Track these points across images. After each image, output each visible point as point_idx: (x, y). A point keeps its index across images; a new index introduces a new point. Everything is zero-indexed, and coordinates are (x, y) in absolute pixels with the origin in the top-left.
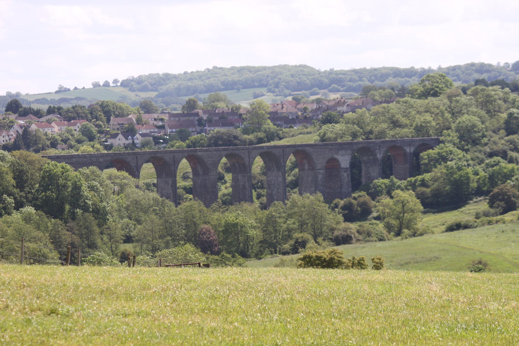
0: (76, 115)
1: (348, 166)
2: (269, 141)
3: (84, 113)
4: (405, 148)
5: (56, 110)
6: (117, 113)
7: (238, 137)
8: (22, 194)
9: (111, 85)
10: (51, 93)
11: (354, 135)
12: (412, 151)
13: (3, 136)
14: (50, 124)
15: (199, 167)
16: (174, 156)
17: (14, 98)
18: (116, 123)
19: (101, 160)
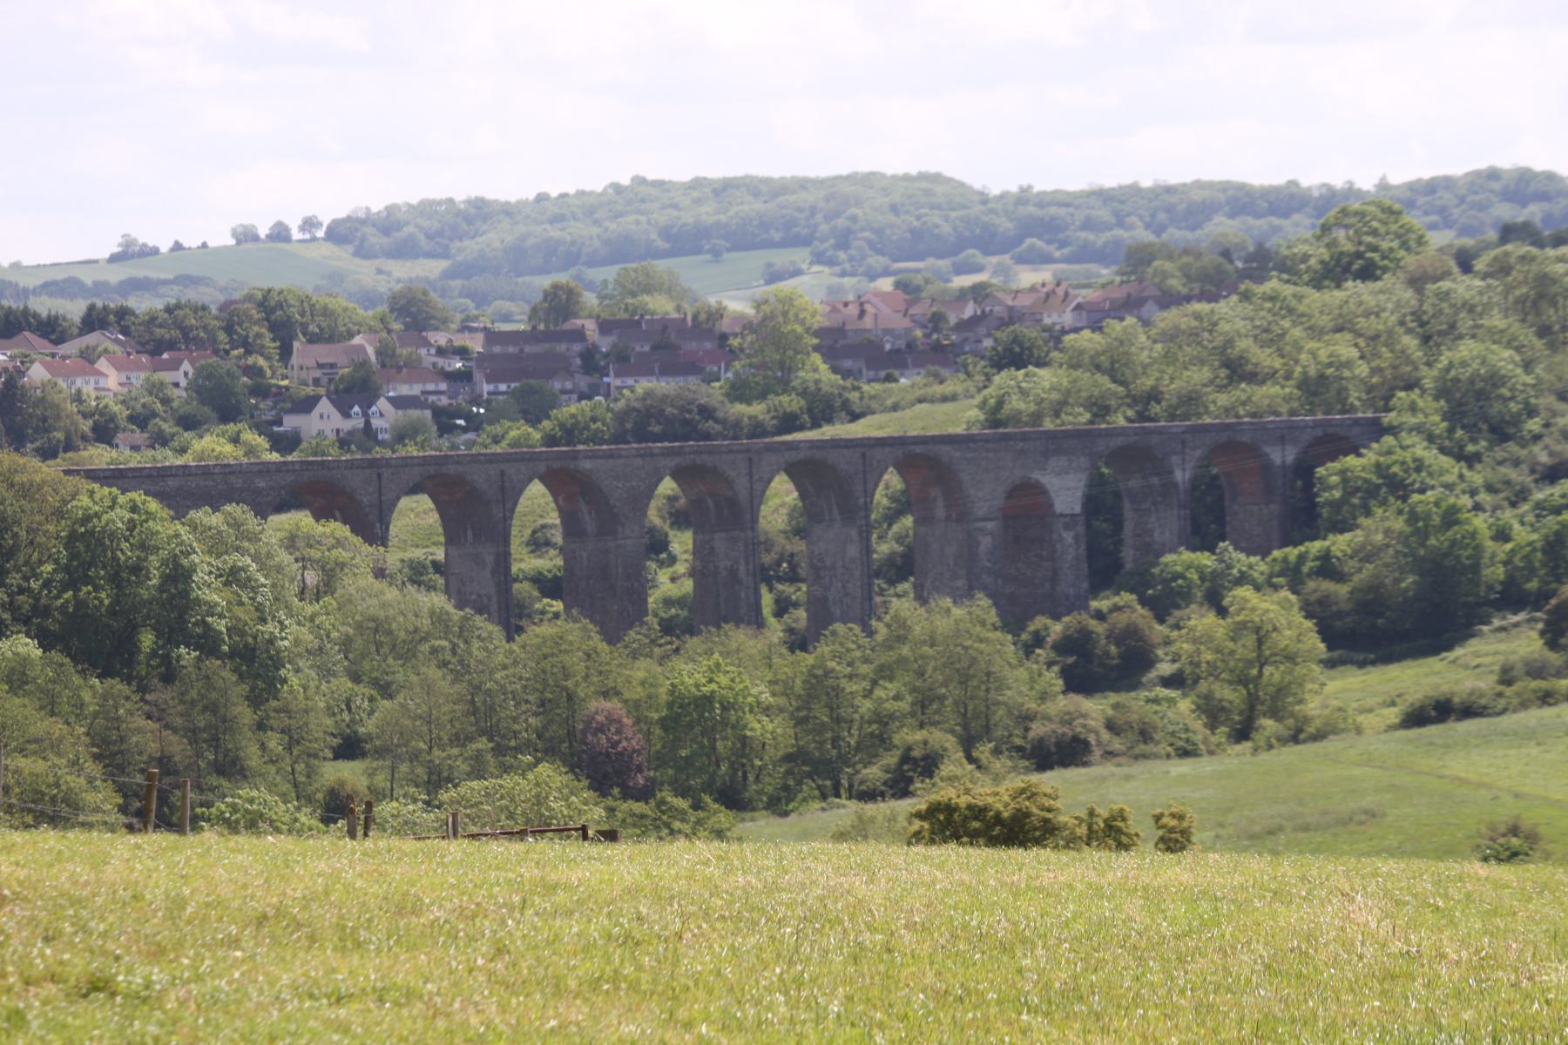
0: (176, 333)
1: (1078, 509)
2: (816, 425)
3: (205, 328)
4: (1268, 449)
6: (313, 328)
7: (715, 410)
9: (296, 235)
10: (96, 262)
11: (1100, 409)
16: (502, 473)
18: (312, 363)
19: (262, 484)
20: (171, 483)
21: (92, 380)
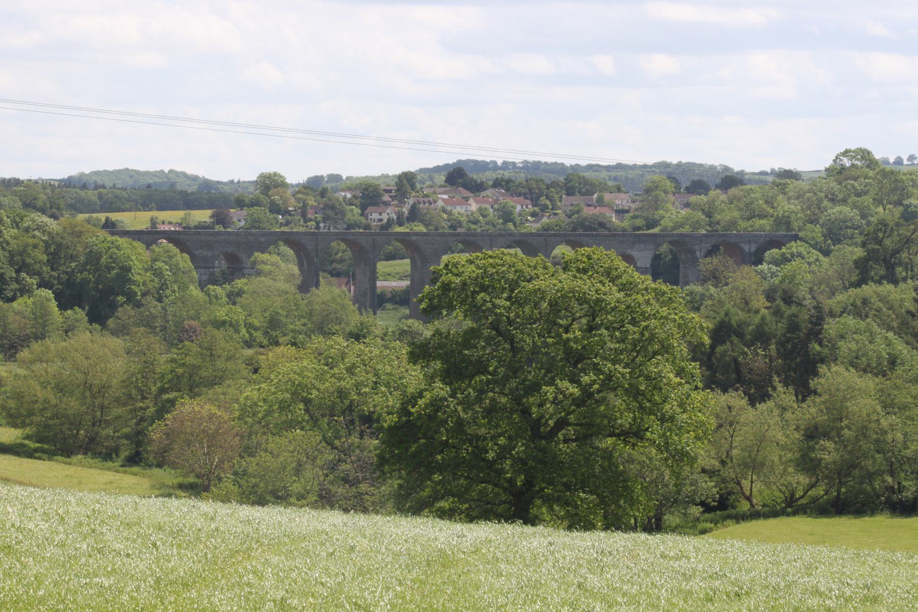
0: (527, 191)
1: (648, 266)
2: (648, 229)
3: (539, 189)
4: (742, 245)
5: (504, 183)
6: (583, 190)
7: (605, 224)
8: (55, 274)
9: (906, 162)
10: (820, 171)
11: (696, 225)
12: (753, 249)
13: (388, 214)
14: (467, 201)
15: (416, 255)
16: (374, 240)
17: (723, 176)
18: (569, 204)
19: (263, 240)
20: (222, 237)
21: (464, 207)
